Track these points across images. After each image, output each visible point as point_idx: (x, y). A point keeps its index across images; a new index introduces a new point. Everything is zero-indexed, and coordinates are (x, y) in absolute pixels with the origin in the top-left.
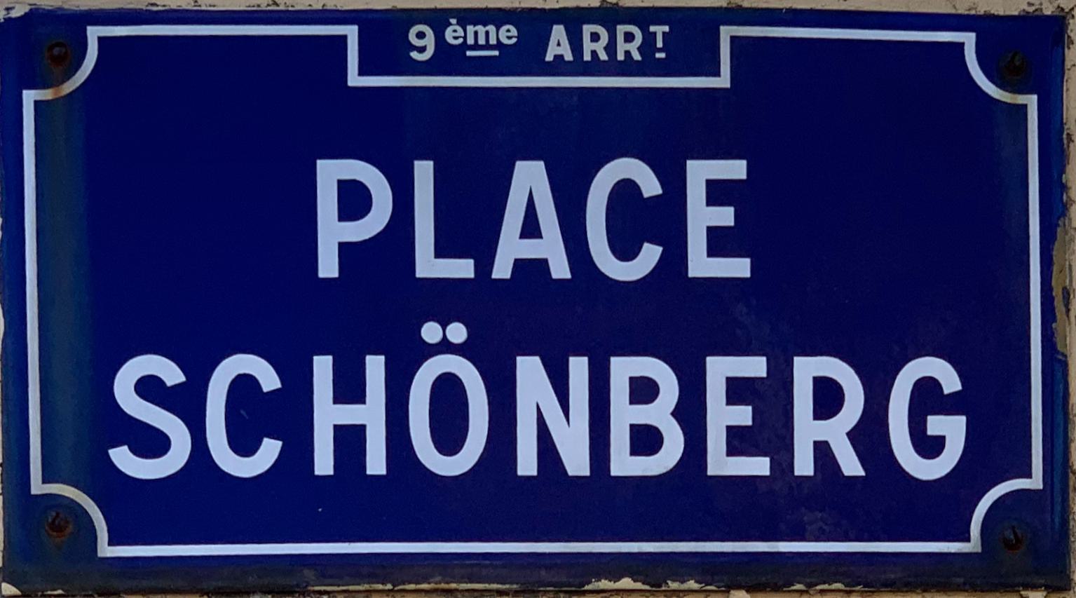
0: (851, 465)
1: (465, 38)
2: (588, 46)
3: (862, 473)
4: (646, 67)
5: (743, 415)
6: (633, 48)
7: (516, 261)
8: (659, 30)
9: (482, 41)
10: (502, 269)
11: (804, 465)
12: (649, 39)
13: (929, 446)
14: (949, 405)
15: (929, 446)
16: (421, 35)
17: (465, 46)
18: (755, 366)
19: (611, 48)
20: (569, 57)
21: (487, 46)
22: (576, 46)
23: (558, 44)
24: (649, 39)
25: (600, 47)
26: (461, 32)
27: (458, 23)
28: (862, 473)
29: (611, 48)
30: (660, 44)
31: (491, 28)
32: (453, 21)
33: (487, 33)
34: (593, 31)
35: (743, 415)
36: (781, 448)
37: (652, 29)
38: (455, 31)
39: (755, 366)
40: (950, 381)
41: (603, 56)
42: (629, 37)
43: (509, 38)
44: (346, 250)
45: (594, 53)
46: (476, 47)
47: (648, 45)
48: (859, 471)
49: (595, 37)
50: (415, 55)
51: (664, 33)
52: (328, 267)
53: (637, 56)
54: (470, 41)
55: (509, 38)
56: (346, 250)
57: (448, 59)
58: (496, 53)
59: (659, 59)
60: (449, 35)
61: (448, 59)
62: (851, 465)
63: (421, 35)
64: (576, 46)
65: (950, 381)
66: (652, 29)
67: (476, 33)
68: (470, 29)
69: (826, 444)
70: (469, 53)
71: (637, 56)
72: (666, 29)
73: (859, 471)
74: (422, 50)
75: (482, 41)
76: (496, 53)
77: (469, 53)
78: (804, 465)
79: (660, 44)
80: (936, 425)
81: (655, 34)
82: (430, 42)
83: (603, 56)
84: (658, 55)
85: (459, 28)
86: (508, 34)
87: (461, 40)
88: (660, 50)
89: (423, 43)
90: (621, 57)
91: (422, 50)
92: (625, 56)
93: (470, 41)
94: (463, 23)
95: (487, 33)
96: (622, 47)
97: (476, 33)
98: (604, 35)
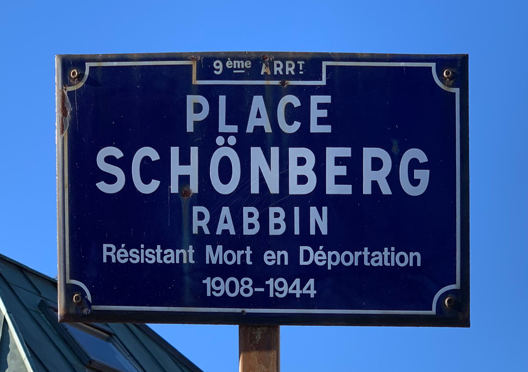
0: (386, 190)
1: (233, 65)
2: (276, 69)
3: (391, 193)
4: (297, 77)
5: (342, 171)
6: (292, 70)
7: (255, 126)
8: (301, 63)
9: (239, 67)
10: (250, 129)
11: (367, 190)
12: (297, 66)
13: (415, 182)
14: (423, 166)
15: (415, 182)
16: (218, 65)
17: (233, 69)
18: (346, 152)
19: (284, 70)
20: (269, 73)
21: (241, 69)
22: (238, 223)
23: (264, 70)
24: (297, 66)
25: (280, 69)
26: (231, 63)
27: (231, 60)
28: (391, 193)
29: (284, 70)
30: (301, 68)
31: (242, 62)
32: (229, 59)
33: (241, 64)
34: (278, 63)
35: (342, 171)
36: (358, 185)
37: (298, 62)
38: (230, 63)
39: (346, 152)
40: (422, 158)
41: (281, 73)
42: (290, 65)
43: (248, 65)
44: (196, 123)
45: (278, 72)
46: (237, 69)
47: (297, 69)
48: (389, 192)
49: (278, 66)
50: (215, 72)
51: (303, 64)
52: (190, 128)
53: (293, 73)
54: (235, 67)
55: (248, 65)
56: (196, 123)
57: (228, 74)
58: (243, 71)
59: (301, 74)
60: (227, 64)
61: (228, 74)
62: (386, 190)
63: (218, 65)
64: (238, 223)
65: (422, 158)
66: (298, 62)
67: (237, 64)
68: (235, 62)
69: (376, 181)
70: (234, 71)
71: (293, 73)
72: (303, 62)
73: (389, 192)
74: (218, 70)
75: (239, 67)
76: (243, 71)
77: (234, 71)
78: (367, 190)
79: (301, 68)
80: (418, 174)
81: (299, 64)
82: (221, 67)
83: (281, 73)
84: (301, 73)
85: (231, 62)
86: (248, 64)
87: (231, 66)
88: (301, 71)
89: (218, 67)
90: (287, 73)
91: (218, 70)
92: (289, 73)
93: (235, 67)
94: (232, 60)
95: (241, 64)
96: (288, 69)
97: (237, 64)
98: (281, 65)
